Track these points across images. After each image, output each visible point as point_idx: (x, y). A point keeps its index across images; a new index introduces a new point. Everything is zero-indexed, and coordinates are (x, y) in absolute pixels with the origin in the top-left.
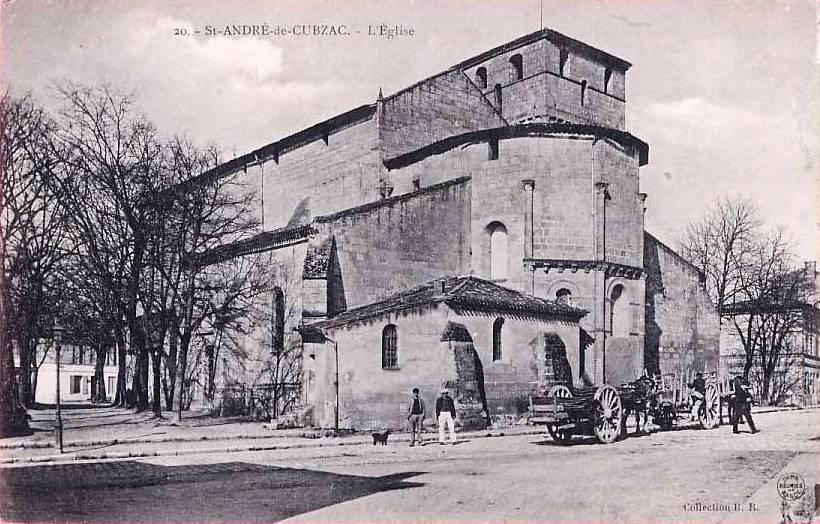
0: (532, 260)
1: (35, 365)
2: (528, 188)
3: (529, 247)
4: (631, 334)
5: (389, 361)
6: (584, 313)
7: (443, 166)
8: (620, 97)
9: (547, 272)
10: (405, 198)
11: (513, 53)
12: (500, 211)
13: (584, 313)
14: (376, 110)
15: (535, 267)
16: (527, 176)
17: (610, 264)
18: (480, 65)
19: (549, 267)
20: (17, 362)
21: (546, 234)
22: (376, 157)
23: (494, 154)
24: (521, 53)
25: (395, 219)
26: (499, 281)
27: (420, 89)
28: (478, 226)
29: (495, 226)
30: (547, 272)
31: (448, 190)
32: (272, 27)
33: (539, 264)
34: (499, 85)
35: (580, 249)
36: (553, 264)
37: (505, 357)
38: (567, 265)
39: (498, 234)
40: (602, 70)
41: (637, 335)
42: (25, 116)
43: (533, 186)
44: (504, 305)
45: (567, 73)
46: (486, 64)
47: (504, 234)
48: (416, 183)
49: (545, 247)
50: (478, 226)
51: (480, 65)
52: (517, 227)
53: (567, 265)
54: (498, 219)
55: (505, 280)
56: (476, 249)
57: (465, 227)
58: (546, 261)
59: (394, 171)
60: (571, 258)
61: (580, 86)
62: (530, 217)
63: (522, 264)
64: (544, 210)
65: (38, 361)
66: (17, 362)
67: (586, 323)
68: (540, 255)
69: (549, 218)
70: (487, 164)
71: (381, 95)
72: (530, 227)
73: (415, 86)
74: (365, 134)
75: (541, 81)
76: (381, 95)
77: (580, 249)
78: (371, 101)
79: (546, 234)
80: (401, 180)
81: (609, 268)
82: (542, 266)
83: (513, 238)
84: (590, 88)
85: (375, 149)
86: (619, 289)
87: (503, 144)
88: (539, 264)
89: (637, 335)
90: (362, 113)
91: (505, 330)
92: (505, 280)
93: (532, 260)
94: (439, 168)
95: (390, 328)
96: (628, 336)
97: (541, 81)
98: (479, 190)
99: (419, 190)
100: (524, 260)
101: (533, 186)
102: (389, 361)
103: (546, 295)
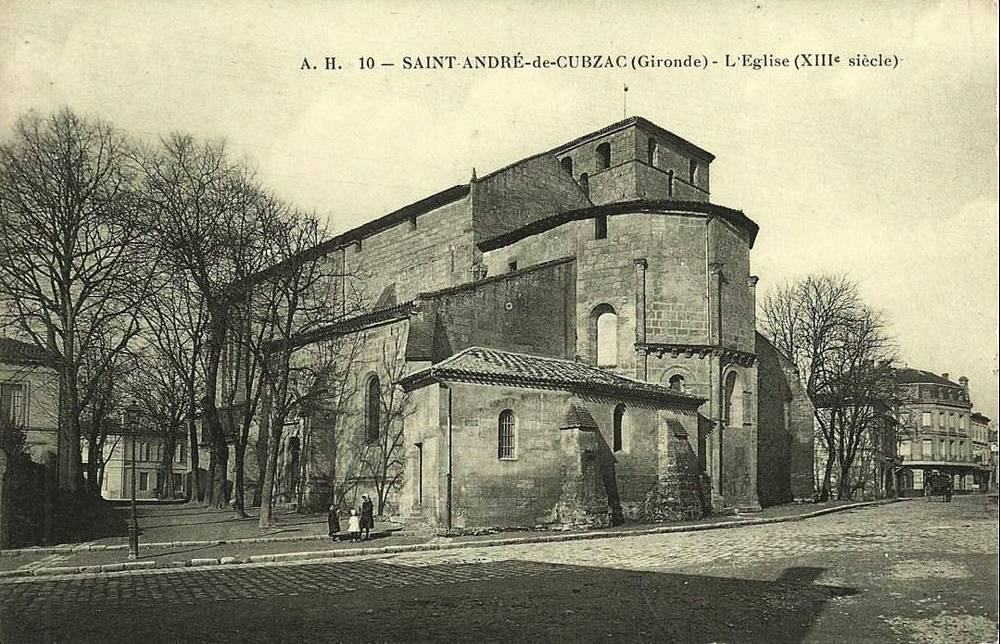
0: (645, 345)
1: (101, 460)
2: (639, 268)
3: (641, 330)
4: (745, 424)
5: (503, 450)
6: (702, 401)
8: (704, 188)
9: (660, 357)
10: (497, 280)
11: (601, 146)
12: (606, 293)
13: (702, 401)
14: (469, 190)
15: (648, 352)
16: (638, 254)
17: (726, 350)
18: (566, 155)
19: (663, 352)
20: (85, 458)
21: (659, 317)
22: (468, 239)
24: (609, 141)
27: (514, 171)
29: (605, 308)
30: (660, 357)
32: (348, 58)
33: (652, 348)
34: (586, 174)
35: (694, 333)
36: (667, 348)
37: (626, 449)
38: (680, 349)
39: (605, 317)
40: (687, 163)
41: (750, 425)
43: (646, 266)
44: (623, 395)
45: (655, 163)
46: (572, 153)
47: (613, 315)
48: (513, 265)
49: (658, 331)
50: (582, 310)
51: (566, 155)
52: (629, 311)
53: (680, 349)
54: (607, 300)
55: (615, 367)
58: (661, 345)
59: (487, 254)
60: (685, 343)
62: (642, 299)
64: (657, 291)
65: (105, 457)
66: (85, 458)
67: (703, 410)
68: (652, 339)
69: (661, 299)
70: (591, 244)
71: (474, 175)
72: (642, 309)
73: (508, 168)
74: (465, 203)
75: (631, 169)
76: (474, 175)
77: (694, 333)
78: (466, 181)
79: (659, 317)
80: (496, 262)
81: (739, 356)
82: (654, 350)
83: (621, 321)
84: (676, 178)
85: (468, 231)
86: (732, 376)
87: (613, 221)
88: (652, 348)
89: (750, 425)
90: (456, 193)
91: (626, 418)
93: (645, 345)
94: (537, 249)
96: (741, 427)
97: (631, 169)
98: (584, 271)
101: (646, 266)
103: (658, 380)
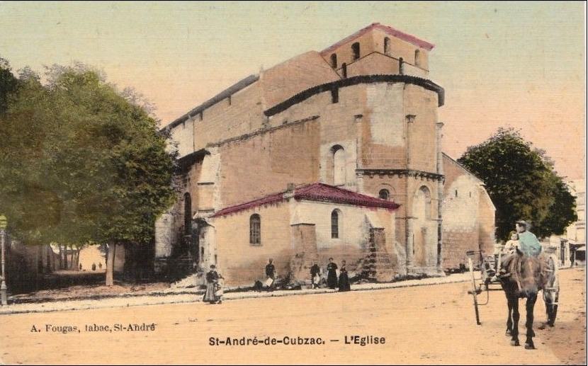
5: (255, 239)
7: (368, 188)
23: (335, 100)
25: (265, 144)
26: (341, 186)
28: (325, 150)
31: (303, 125)
39: (339, 153)
42: (457, 205)
50: (325, 150)
56: (323, 163)
57: (409, 205)
58: (391, 170)
61: (398, 62)
63: (355, 173)
70: (330, 107)
92: (343, 185)
95: (256, 217)
99: (286, 124)
100: (357, 170)
102: (255, 239)
